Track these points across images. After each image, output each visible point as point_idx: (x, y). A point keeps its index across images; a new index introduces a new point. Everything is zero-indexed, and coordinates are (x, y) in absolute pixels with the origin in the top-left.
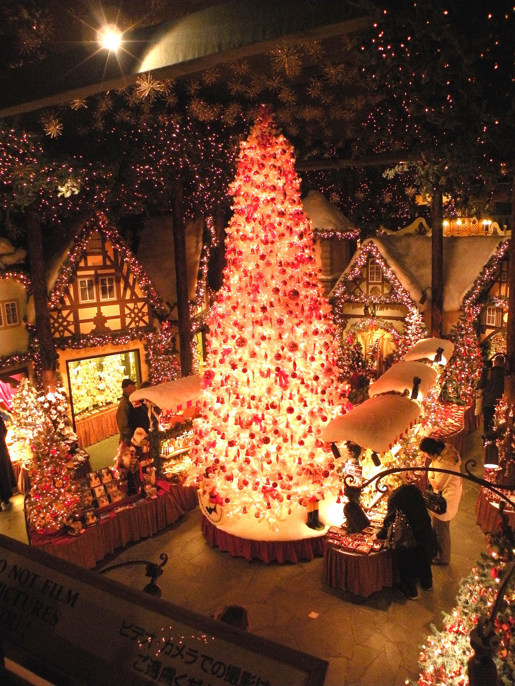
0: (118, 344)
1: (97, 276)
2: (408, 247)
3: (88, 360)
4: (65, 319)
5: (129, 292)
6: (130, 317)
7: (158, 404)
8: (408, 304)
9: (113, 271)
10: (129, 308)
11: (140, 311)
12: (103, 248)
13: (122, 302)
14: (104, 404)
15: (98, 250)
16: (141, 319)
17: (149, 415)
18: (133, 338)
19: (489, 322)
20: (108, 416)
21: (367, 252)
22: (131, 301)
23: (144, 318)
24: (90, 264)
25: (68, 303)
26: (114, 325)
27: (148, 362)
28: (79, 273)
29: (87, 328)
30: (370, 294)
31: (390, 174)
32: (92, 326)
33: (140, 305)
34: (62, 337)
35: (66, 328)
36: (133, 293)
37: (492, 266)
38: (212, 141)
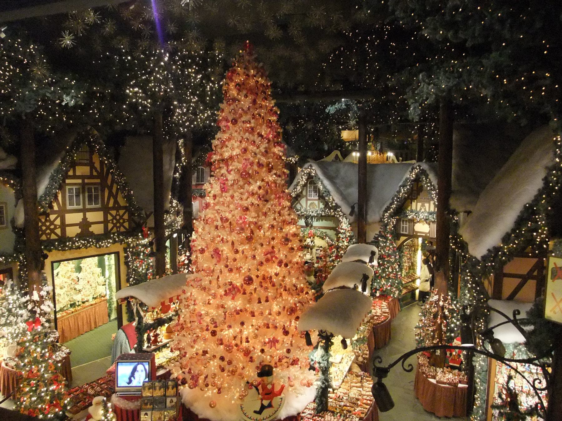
0: (100, 246)
1: (83, 185)
2: (338, 171)
3: (66, 262)
4: (52, 223)
5: (112, 201)
6: (112, 223)
7: (144, 301)
8: (340, 216)
9: (98, 181)
10: (111, 215)
11: (121, 217)
12: (91, 158)
13: (105, 209)
14: (80, 303)
15: (86, 162)
16: (122, 225)
17: (135, 311)
18: (115, 242)
19: (403, 231)
20: (84, 314)
21: (307, 173)
22: (113, 208)
23: (124, 224)
24: (78, 173)
25: (56, 208)
26: (97, 229)
27: (127, 263)
28: (68, 181)
29: (72, 232)
30: (308, 208)
31: (331, 109)
32: (77, 230)
33: (121, 212)
34: (48, 239)
35: (53, 231)
36: (116, 202)
37: (407, 186)
38: (192, 72)
